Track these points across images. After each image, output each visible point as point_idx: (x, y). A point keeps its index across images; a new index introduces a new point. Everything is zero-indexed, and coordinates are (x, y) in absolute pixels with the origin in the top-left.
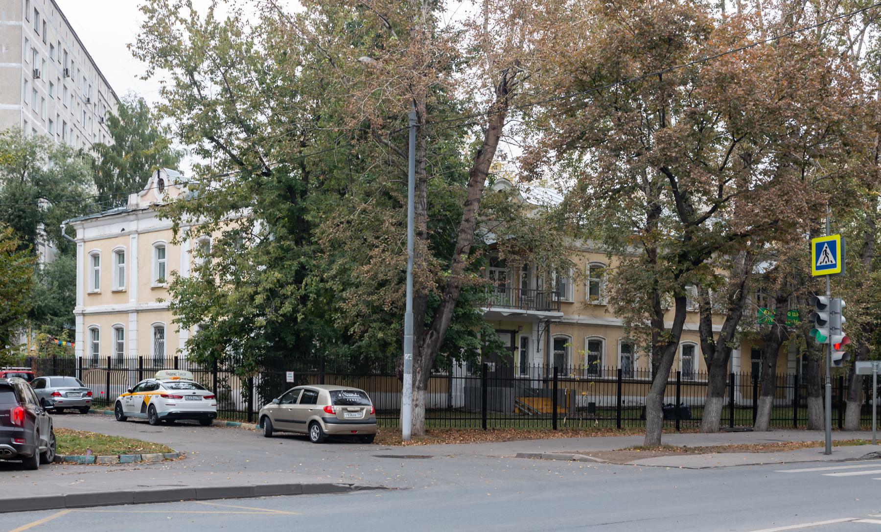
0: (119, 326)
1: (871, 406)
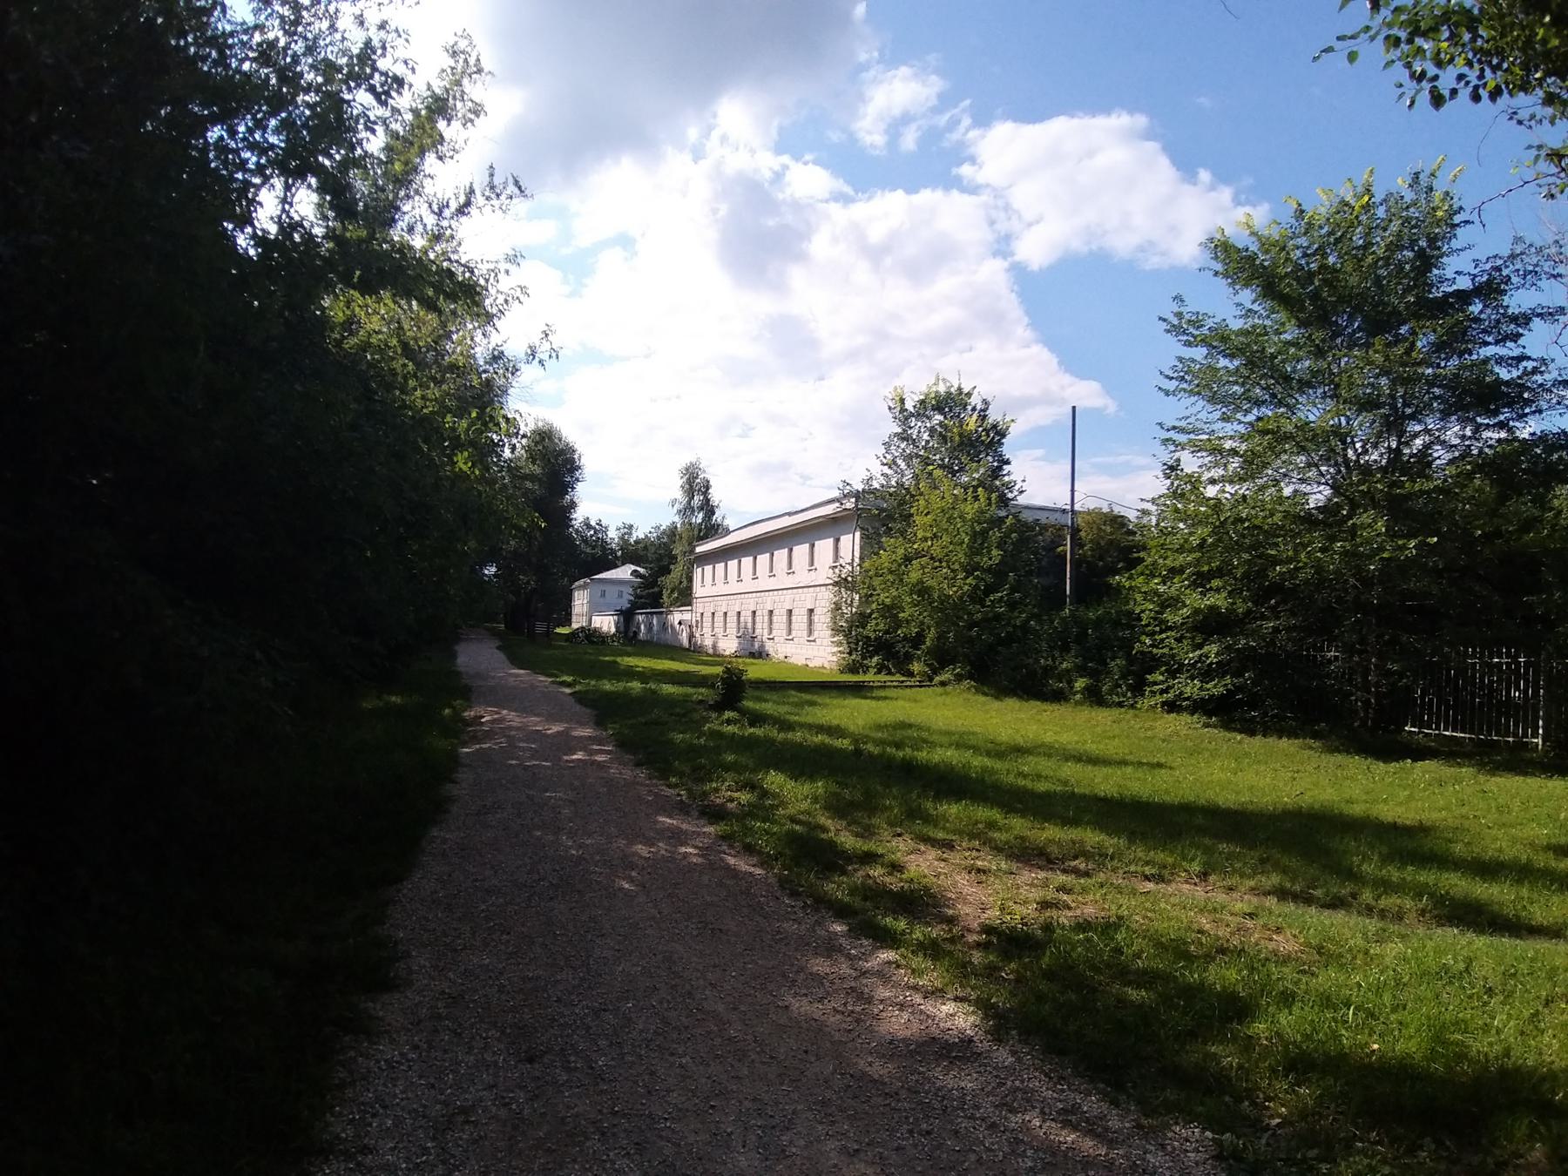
0: (570, 432)
1: (599, 677)
